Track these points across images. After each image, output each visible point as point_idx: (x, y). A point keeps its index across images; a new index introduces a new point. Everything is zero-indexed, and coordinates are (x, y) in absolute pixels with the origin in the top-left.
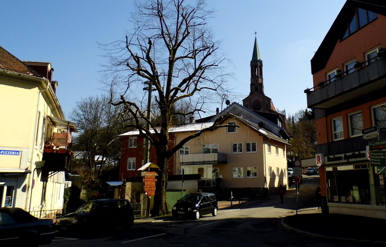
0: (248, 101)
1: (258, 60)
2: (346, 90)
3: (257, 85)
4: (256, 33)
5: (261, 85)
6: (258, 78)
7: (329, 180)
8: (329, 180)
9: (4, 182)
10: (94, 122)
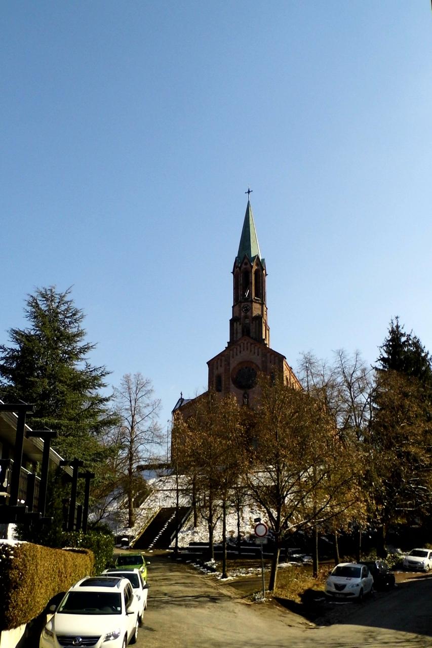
0: (223, 364)
3: (247, 321)
4: (249, 192)
5: (259, 320)
6: (252, 301)
7: (40, 479)
8: (40, 479)
9: (73, 476)
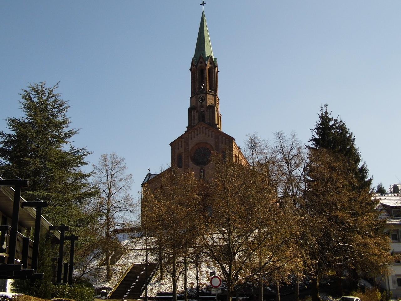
1: (207, 56)
2: (12, 208)
3: (203, 110)
4: (203, 4)
5: (213, 109)
6: (206, 93)
10: (253, 196)
